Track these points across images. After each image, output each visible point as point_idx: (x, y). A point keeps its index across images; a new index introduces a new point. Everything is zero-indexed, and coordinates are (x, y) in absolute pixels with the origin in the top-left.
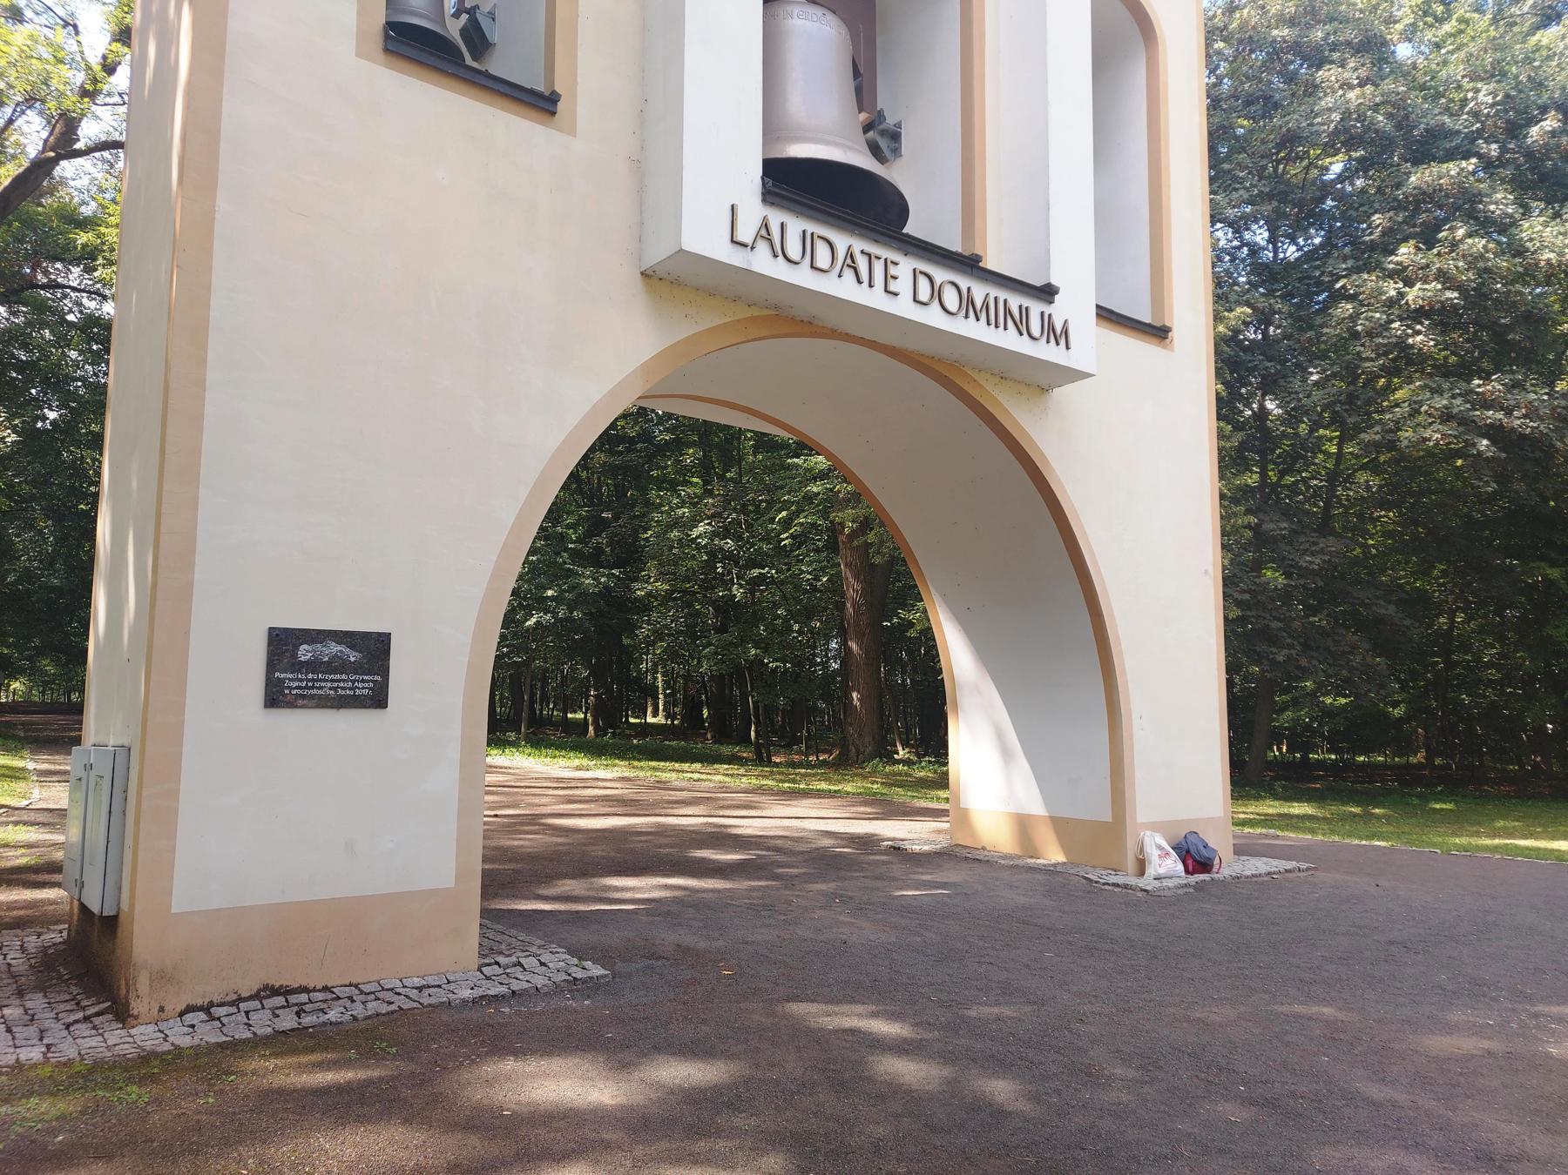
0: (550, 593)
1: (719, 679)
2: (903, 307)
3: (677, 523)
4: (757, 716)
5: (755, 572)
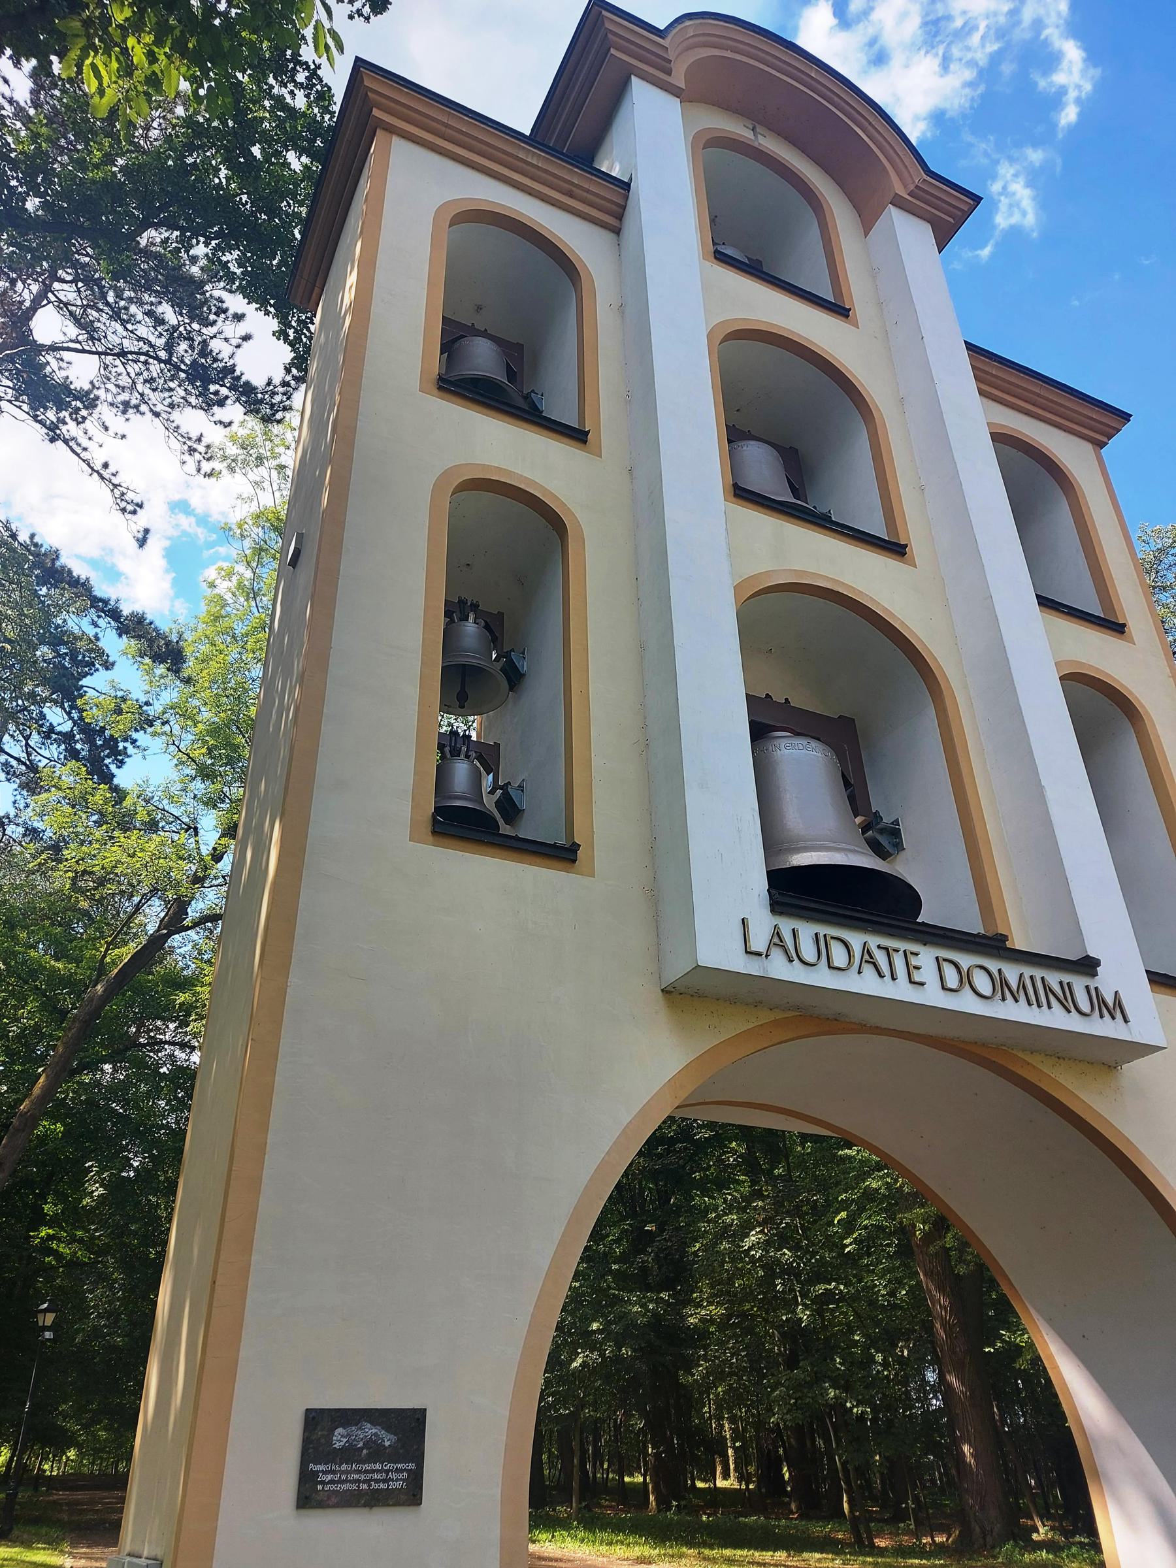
0: (595, 1326)
1: (798, 1430)
2: (932, 996)
3: (725, 1232)
4: (848, 1483)
5: (821, 1288)
